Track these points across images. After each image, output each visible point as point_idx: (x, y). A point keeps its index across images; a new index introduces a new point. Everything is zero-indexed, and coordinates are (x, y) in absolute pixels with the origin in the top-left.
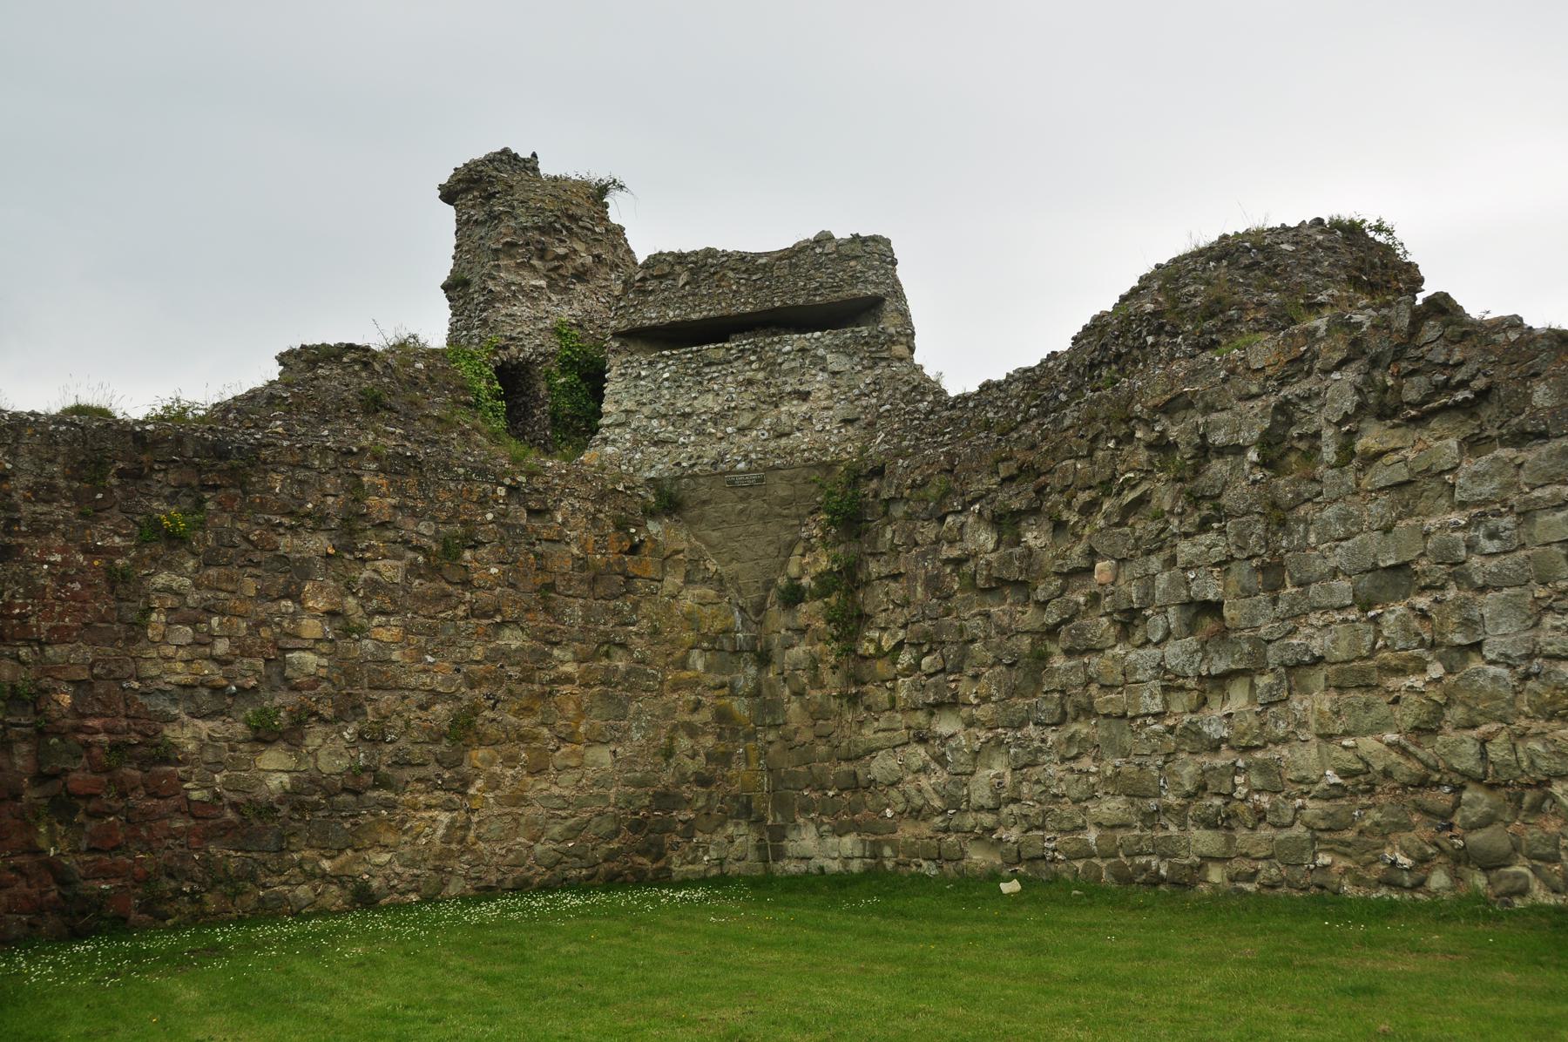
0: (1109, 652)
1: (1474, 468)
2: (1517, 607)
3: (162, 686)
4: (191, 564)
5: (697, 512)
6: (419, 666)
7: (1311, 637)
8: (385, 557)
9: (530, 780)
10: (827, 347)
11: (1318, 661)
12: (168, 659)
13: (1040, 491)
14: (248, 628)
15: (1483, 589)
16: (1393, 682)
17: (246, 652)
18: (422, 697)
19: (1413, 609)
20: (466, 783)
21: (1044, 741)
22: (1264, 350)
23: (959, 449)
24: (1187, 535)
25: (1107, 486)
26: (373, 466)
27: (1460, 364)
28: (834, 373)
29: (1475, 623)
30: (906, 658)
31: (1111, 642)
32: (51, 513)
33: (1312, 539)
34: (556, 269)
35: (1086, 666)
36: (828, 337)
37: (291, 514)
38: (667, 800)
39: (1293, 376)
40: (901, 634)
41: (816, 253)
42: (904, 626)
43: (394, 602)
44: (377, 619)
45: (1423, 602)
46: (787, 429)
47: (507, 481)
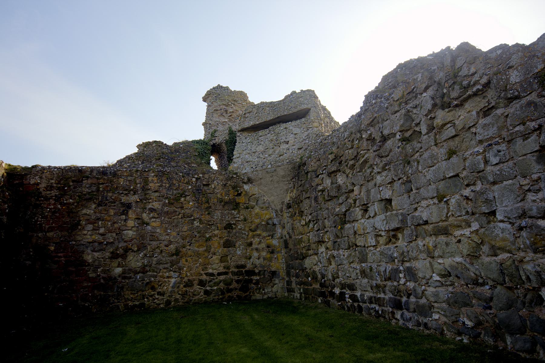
0: (359, 221)
1: (484, 122)
2: (511, 191)
3: (82, 242)
4: (94, 206)
6: (165, 233)
7: (422, 212)
8: (156, 201)
13: (340, 163)
14: (111, 224)
15: (494, 183)
16: (458, 233)
17: (110, 232)
19: (462, 196)
26: (153, 175)
27: (473, 74)
28: (295, 134)
29: (491, 201)
31: (360, 217)
32: (51, 194)
33: (420, 168)
34: (231, 116)
35: (354, 227)
37: (126, 190)
39: (410, 100)
41: (293, 97)
42: (311, 214)
44: (153, 220)
45: (467, 192)
46: (282, 154)
47: (196, 176)
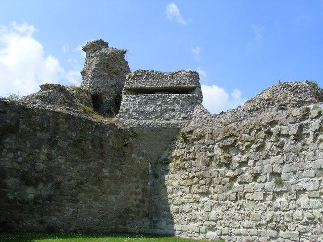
5: (142, 137)
9: (94, 202)
11: (305, 190)
12: (7, 161)
18: (69, 178)
20: (78, 201)
21: (231, 204)
22: (297, 112)
23: (214, 127)
24: (273, 156)
25: (253, 142)
30: (196, 179)
34: (110, 71)
36: (181, 95)
38: (127, 211)
40: (194, 174)
43: (64, 153)
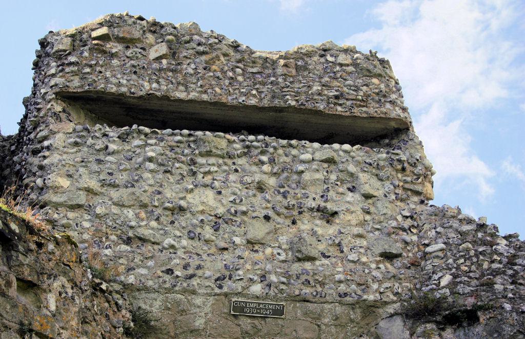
10: (358, 163)
28: (367, 197)
36: (358, 152)
